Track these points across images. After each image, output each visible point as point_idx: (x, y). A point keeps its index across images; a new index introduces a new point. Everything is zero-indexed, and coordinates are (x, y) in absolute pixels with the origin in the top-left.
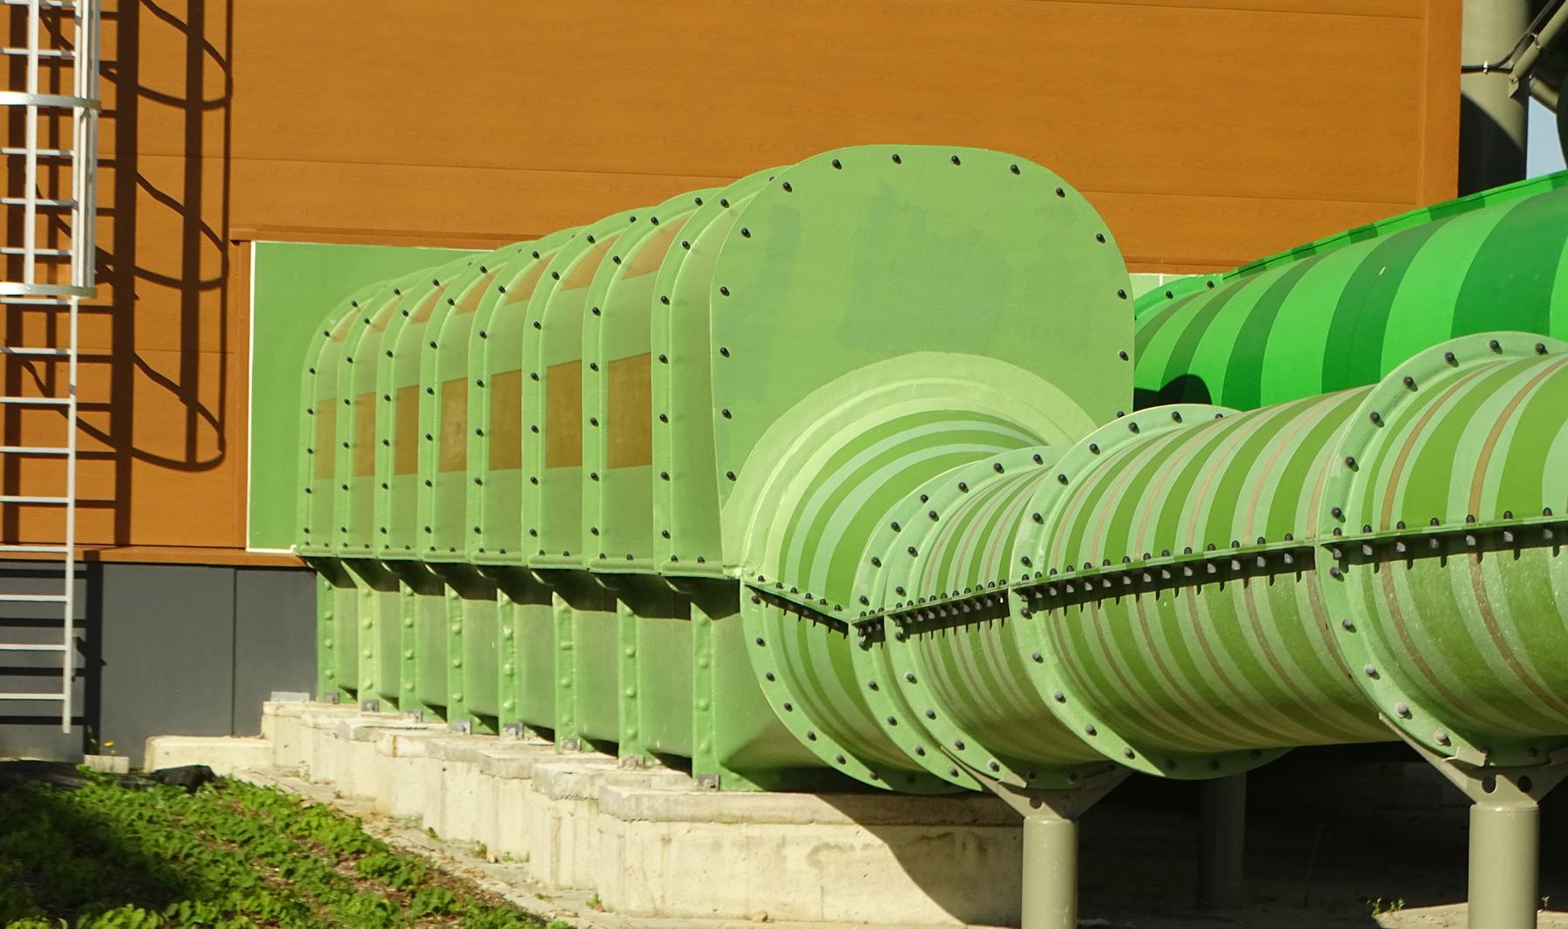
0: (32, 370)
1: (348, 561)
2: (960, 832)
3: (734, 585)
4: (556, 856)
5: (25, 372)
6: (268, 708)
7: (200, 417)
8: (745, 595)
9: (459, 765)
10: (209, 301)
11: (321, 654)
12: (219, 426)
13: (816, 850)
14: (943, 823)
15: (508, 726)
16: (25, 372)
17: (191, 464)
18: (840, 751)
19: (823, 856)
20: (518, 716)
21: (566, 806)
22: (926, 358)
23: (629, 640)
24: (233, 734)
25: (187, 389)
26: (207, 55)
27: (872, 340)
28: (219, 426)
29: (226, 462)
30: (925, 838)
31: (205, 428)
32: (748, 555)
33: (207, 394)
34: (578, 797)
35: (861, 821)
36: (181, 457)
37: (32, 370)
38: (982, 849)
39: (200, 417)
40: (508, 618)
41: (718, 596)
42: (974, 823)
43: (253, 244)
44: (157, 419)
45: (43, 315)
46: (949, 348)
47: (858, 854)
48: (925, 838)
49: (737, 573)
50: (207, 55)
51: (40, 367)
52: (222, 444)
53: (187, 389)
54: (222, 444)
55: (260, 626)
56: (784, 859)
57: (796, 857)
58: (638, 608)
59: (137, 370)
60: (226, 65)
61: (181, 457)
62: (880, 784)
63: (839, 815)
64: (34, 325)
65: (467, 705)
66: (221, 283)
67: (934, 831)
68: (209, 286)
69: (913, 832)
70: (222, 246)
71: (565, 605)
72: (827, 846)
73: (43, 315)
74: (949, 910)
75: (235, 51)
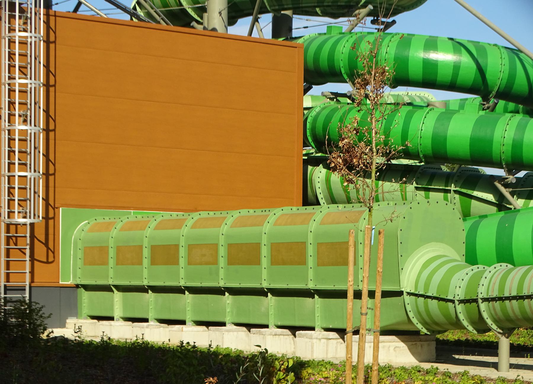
0: (12, 239)
1: (113, 286)
2: (418, 343)
3: (403, 292)
4: (312, 352)
5: (11, 240)
6: (68, 321)
7: (49, 251)
8: (405, 294)
9: (227, 333)
10: (51, 222)
11: (83, 307)
12: (53, 253)
13: (395, 348)
14: (415, 341)
15: (229, 323)
16: (11, 240)
17: (48, 262)
18: (422, 327)
19: (396, 349)
20: (230, 321)
21: (315, 341)
22: (433, 243)
23: (318, 304)
24: (60, 328)
25: (46, 244)
26: (50, 163)
27: (425, 240)
28: (53, 253)
29: (55, 262)
30: (412, 344)
31: (51, 254)
32: (407, 284)
33: (51, 246)
34: (317, 338)
35: (403, 341)
36: (45, 260)
37: (12, 239)
38: (422, 346)
39: (49, 251)
40: (228, 298)
41: (400, 294)
42: (420, 341)
43: (61, 209)
44: (40, 251)
45: (14, 226)
46: (437, 242)
47: (402, 348)
48: (412, 344)
49: (403, 290)
50: (50, 163)
51: (14, 238)
52: (54, 257)
53: (46, 244)
54: (54, 257)
55: (67, 298)
56: (389, 350)
57: (392, 349)
58: (320, 297)
59: (35, 239)
60: (54, 165)
61: (45, 260)
62: (428, 333)
63: (398, 340)
64: (12, 228)
65: (190, 319)
66: (53, 218)
67: (414, 343)
68: (51, 219)
69: (410, 343)
70: (54, 209)
71: (271, 296)
72: (396, 347)
73: (14, 226)
74: (417, 359)
75: (56, 162)
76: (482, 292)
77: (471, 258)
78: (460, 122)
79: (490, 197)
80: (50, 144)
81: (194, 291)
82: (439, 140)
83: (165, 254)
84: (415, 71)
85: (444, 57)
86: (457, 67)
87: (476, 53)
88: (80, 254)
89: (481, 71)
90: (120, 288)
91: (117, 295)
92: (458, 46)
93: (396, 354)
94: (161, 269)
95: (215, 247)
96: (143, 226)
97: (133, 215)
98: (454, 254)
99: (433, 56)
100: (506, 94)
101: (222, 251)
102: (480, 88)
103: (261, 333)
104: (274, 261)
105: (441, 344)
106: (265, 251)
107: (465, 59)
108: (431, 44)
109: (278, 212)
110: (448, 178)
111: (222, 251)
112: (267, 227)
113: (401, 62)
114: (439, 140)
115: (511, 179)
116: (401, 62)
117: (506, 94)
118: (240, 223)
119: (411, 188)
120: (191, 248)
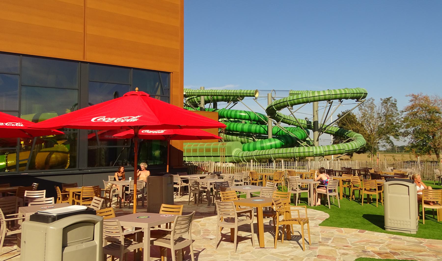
27: (236, 148)
32: (233, 155)
76: (244, 156)
77: (244, 150)
78: (246, 126)
79: (252, 139)
80: (182, 134)
81: (200, 156)
82: (242, 129)
83: (195, 150)
84: (238, 117)
85: (243, 114)
86: (245, 116)
87: (249, 113)
88: (90, 168)
89: (250, 116)
90: (187, 157)
91: (187, 158)
92: (245, 112)
93: (231, 165)
94: (194, 153)
95: (203, 149)
96: (191, 146)
97: (106, 121)
98: (241, 150)
99: (241, 114)
100: (254, 120)
101: (204, 150)
102: (249, 119)
103: (245, 242)
104: (213, 151)
105: (237, 162)
106: (211, 150)
107: (247, 114)
108: (241, 112)
109: (213, 143)
110: (244, 136)
111: (204, 150)
112: (212, 146)
113: (235, 115)
114: (242, 129)
115: (255, 136)
116: (235, 115)
117: (254, 120)
118: (207, 145)
119: (238, 137)
120: (199, 149)
